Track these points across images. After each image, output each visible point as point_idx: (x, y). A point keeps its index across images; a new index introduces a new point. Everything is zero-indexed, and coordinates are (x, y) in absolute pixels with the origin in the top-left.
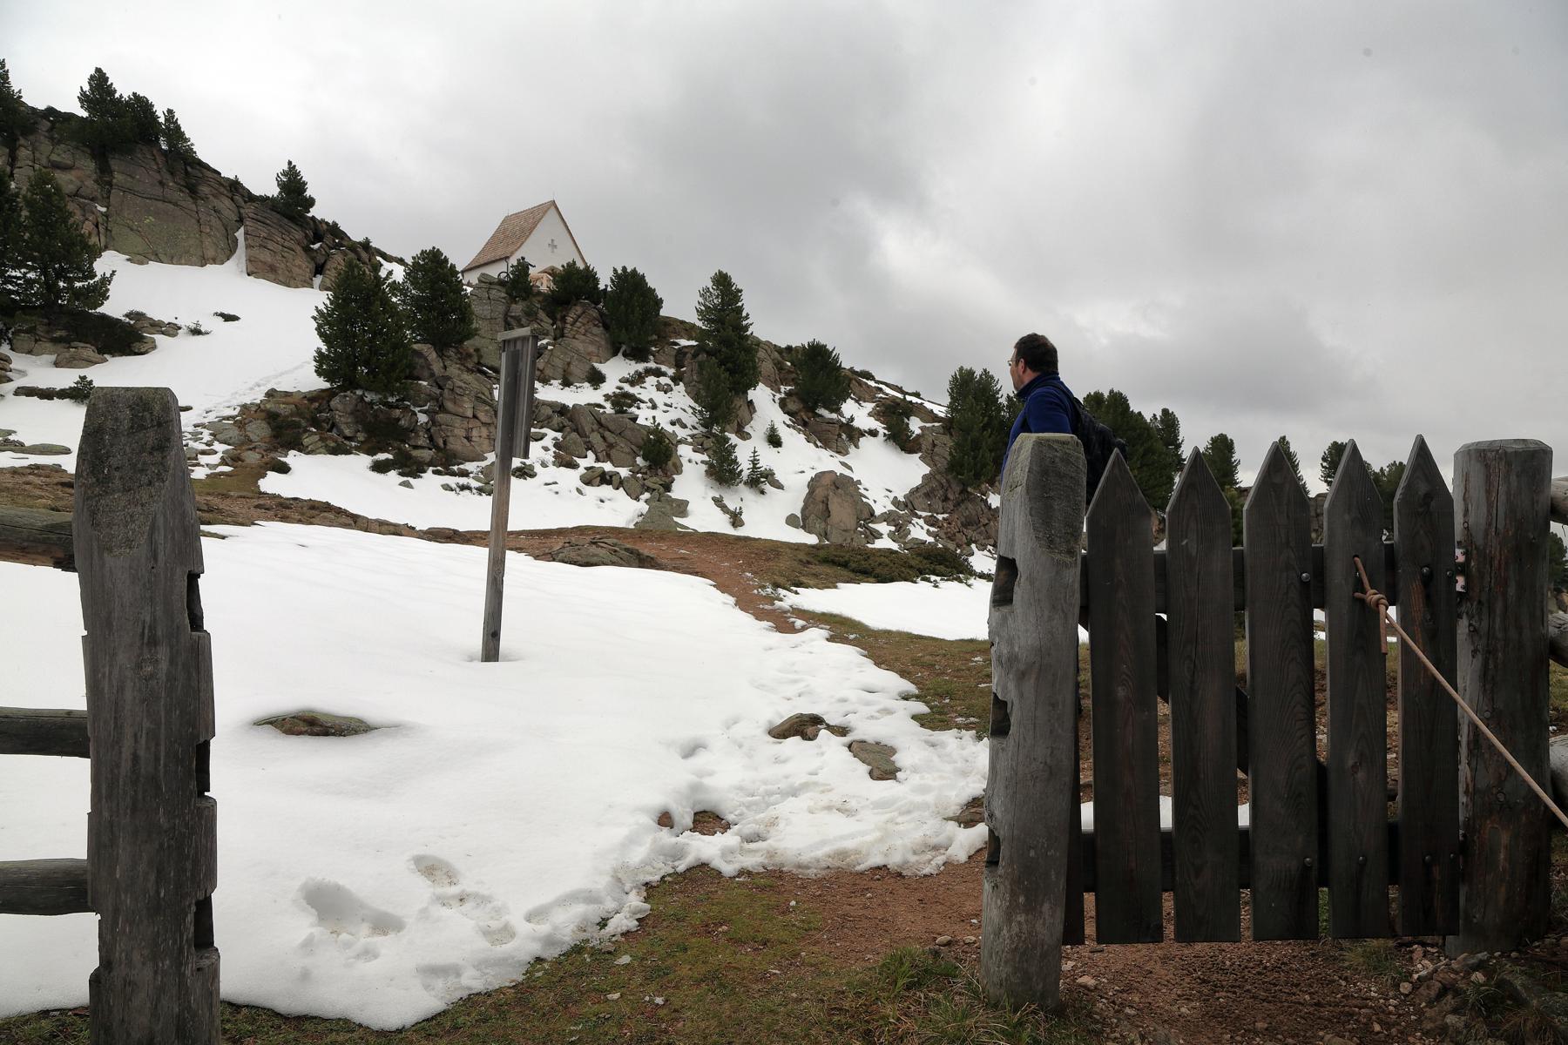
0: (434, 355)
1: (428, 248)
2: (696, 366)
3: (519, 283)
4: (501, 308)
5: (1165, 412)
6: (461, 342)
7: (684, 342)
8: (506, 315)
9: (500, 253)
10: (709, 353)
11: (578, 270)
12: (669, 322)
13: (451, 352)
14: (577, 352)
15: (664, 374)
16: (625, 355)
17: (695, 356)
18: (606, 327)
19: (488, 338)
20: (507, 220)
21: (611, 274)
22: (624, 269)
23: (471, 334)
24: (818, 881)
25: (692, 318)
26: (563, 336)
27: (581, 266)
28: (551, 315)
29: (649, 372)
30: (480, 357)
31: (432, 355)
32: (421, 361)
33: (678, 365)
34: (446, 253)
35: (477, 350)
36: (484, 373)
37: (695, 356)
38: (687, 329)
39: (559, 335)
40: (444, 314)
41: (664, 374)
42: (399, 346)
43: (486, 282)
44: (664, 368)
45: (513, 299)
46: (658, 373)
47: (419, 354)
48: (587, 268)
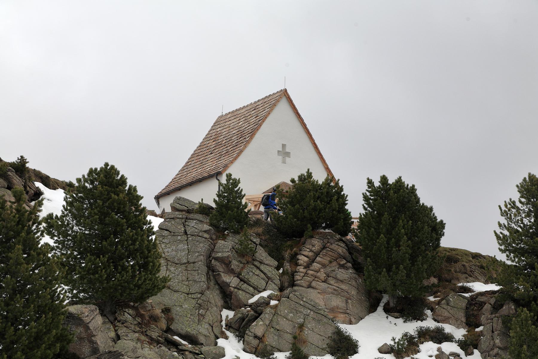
0: (99, 320)
1: (99, 165)
2: (498, 325)
3: (229, 213)
4: (203, 247)
5: (413, 186)
6: (142, 298)
7: (479, 287)
8: (209, 257)
9: (209, 167)
10: (518, 302)
11: (316, 187)
12: (454, 257)
13: (128, 315)
14: (315, 309)
15: (449, 338)
16: (388, 310)
17: (497, 307)
18: (358, 268)
19: (179, 292)
20: (221, 121)
21: (364, 188)
22: (384, 179)
23: (156, 287)
24: (433, 331)
25: (491, 249)
26: (293, 284)
27: (320, 177)
28: (276, 254)
29: (425, 335)
30: (170, 320)
31: (96, 321)
32: (79, 330)
33: (471, 323)
34: (123, 170)
35: (167, 311)
36: (176, 345)
37: (497, 307)
38: (483, 266)
39: (287, 283)
40: (116, 261)
41: (449, 338)
42: (51, 308)
43: (186, 212)
44: (448, 328)
45: (219, 232)
46: (439, 337)
47: (76, 319)
48: (331, 178)
